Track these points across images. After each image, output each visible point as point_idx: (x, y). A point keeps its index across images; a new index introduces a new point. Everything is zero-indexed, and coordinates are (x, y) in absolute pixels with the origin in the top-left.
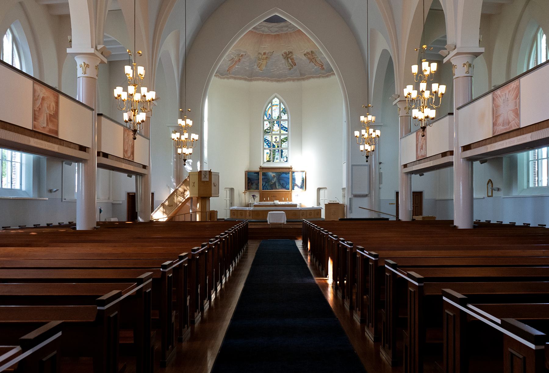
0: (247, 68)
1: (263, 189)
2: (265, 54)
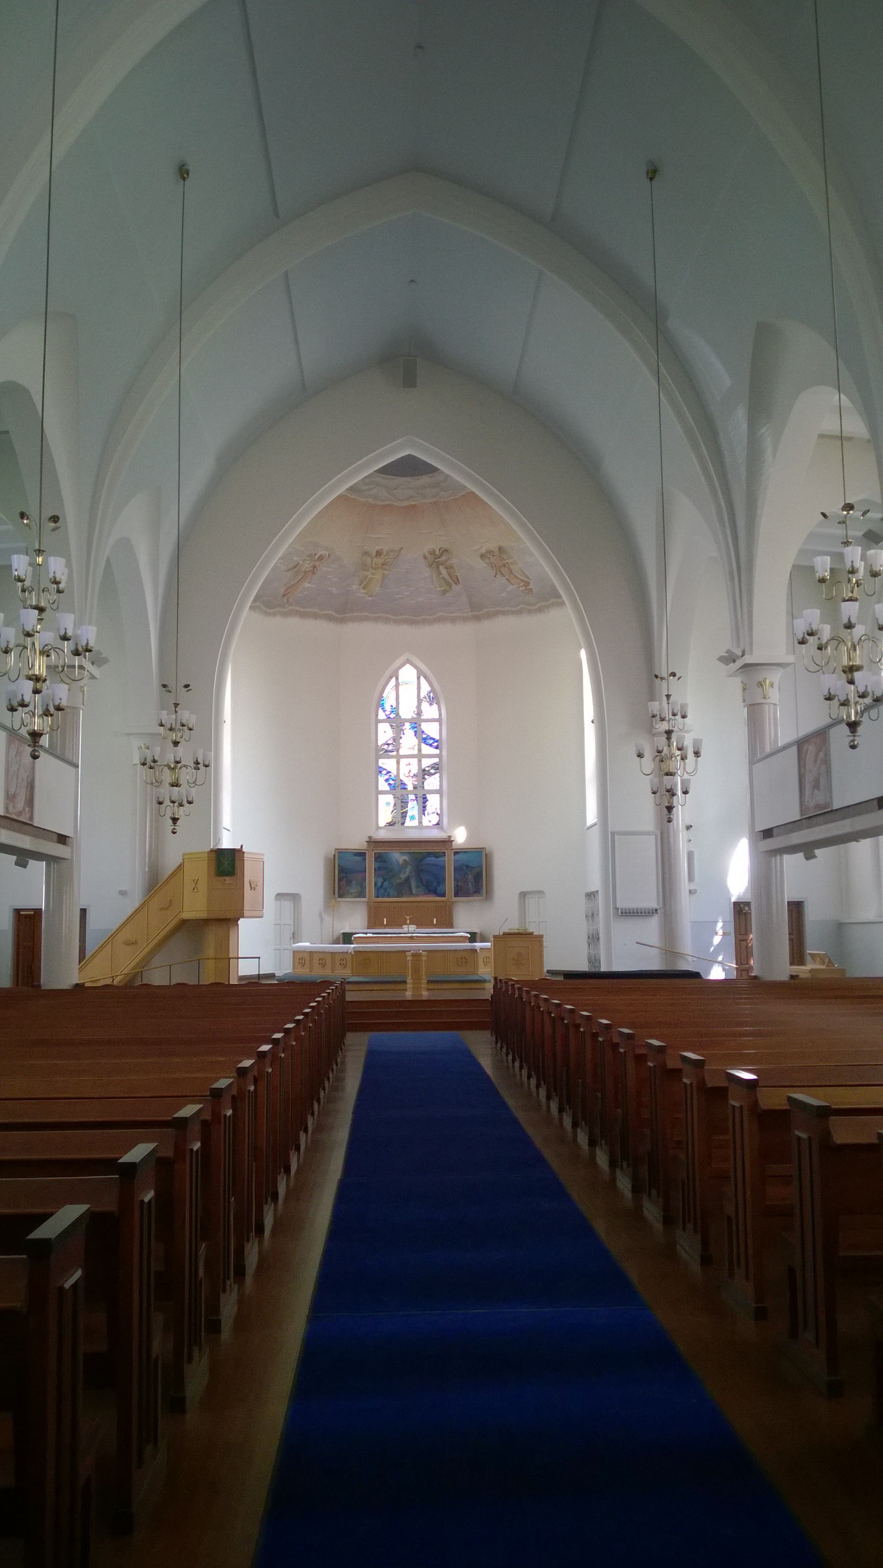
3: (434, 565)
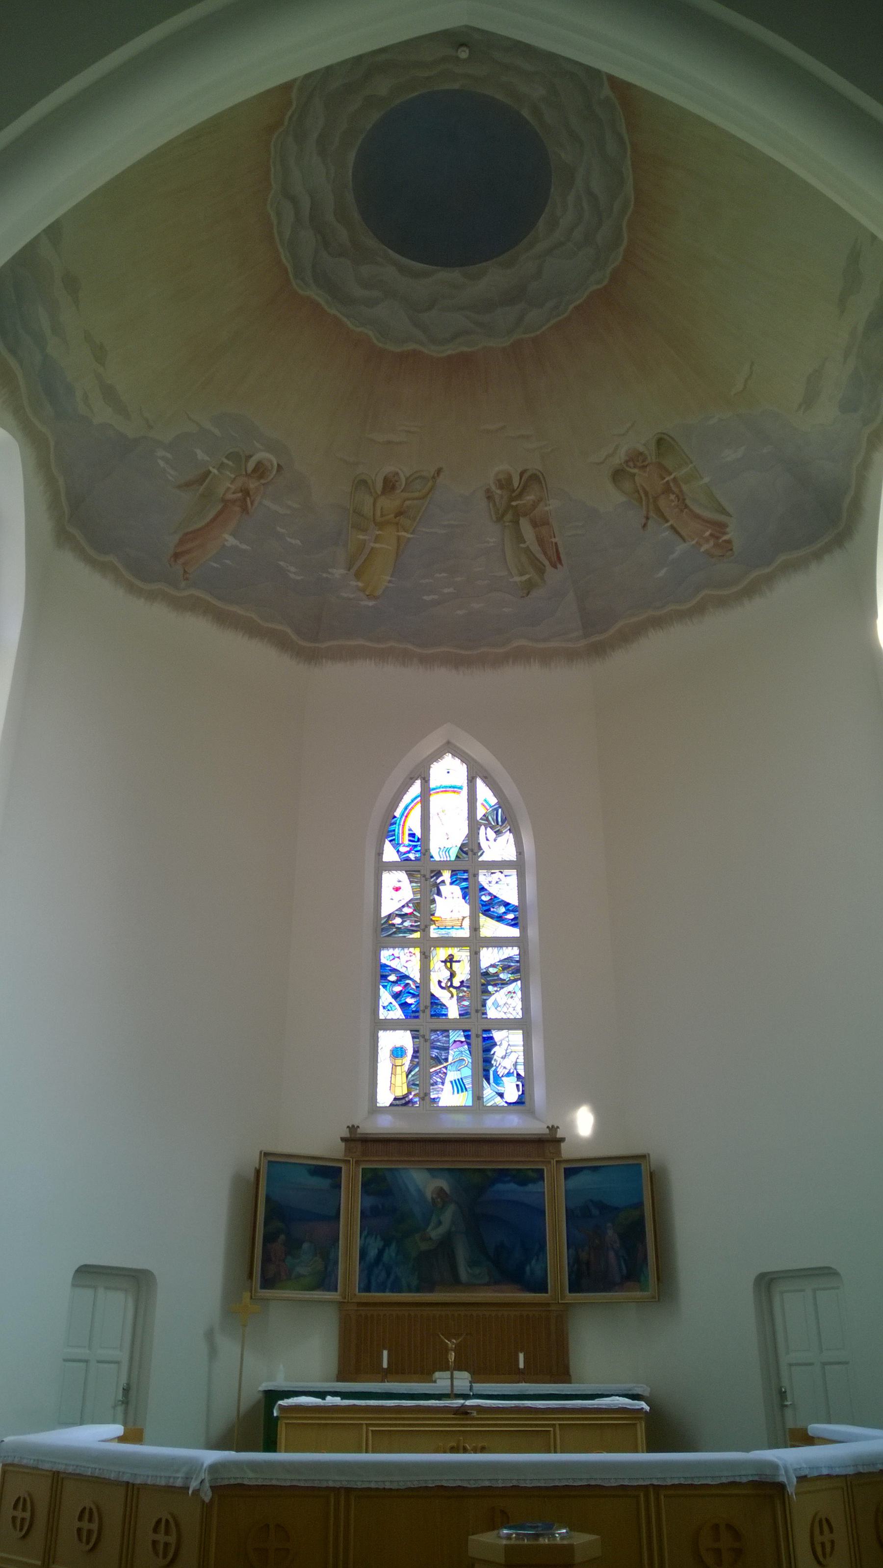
0: (293, 569)
1: (367, 1289)
2: (393, 488)
3: (508, 517)
